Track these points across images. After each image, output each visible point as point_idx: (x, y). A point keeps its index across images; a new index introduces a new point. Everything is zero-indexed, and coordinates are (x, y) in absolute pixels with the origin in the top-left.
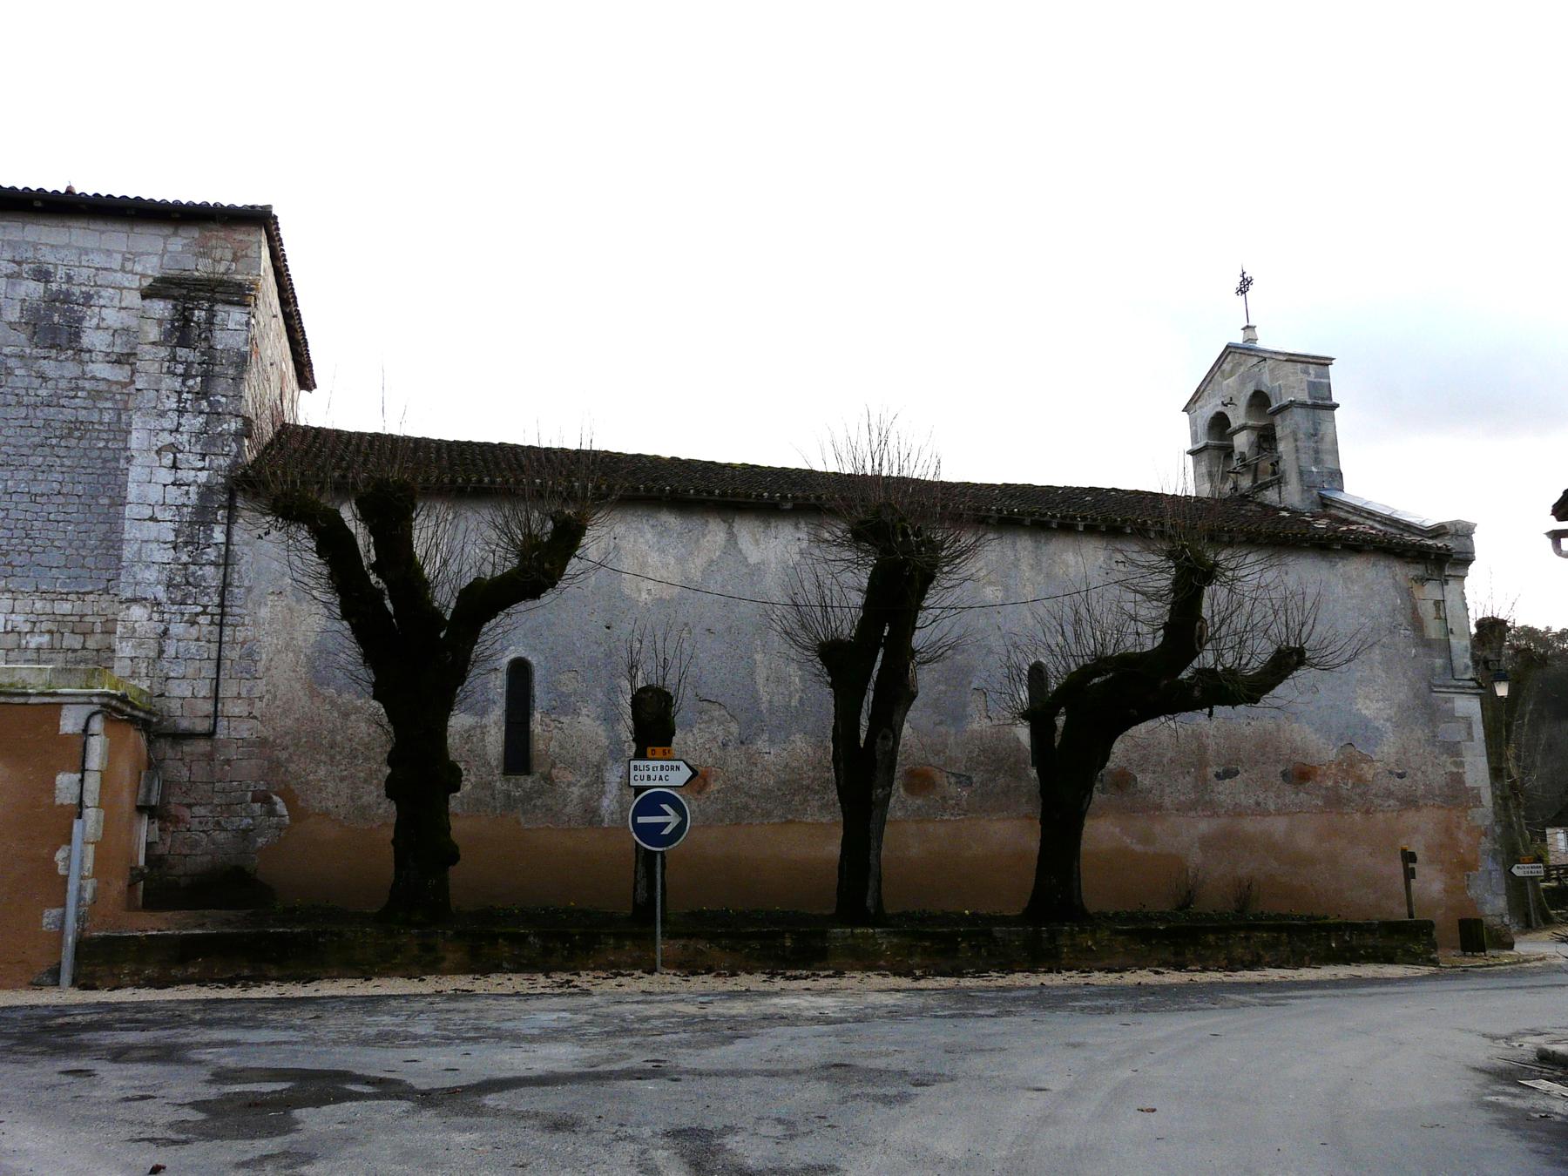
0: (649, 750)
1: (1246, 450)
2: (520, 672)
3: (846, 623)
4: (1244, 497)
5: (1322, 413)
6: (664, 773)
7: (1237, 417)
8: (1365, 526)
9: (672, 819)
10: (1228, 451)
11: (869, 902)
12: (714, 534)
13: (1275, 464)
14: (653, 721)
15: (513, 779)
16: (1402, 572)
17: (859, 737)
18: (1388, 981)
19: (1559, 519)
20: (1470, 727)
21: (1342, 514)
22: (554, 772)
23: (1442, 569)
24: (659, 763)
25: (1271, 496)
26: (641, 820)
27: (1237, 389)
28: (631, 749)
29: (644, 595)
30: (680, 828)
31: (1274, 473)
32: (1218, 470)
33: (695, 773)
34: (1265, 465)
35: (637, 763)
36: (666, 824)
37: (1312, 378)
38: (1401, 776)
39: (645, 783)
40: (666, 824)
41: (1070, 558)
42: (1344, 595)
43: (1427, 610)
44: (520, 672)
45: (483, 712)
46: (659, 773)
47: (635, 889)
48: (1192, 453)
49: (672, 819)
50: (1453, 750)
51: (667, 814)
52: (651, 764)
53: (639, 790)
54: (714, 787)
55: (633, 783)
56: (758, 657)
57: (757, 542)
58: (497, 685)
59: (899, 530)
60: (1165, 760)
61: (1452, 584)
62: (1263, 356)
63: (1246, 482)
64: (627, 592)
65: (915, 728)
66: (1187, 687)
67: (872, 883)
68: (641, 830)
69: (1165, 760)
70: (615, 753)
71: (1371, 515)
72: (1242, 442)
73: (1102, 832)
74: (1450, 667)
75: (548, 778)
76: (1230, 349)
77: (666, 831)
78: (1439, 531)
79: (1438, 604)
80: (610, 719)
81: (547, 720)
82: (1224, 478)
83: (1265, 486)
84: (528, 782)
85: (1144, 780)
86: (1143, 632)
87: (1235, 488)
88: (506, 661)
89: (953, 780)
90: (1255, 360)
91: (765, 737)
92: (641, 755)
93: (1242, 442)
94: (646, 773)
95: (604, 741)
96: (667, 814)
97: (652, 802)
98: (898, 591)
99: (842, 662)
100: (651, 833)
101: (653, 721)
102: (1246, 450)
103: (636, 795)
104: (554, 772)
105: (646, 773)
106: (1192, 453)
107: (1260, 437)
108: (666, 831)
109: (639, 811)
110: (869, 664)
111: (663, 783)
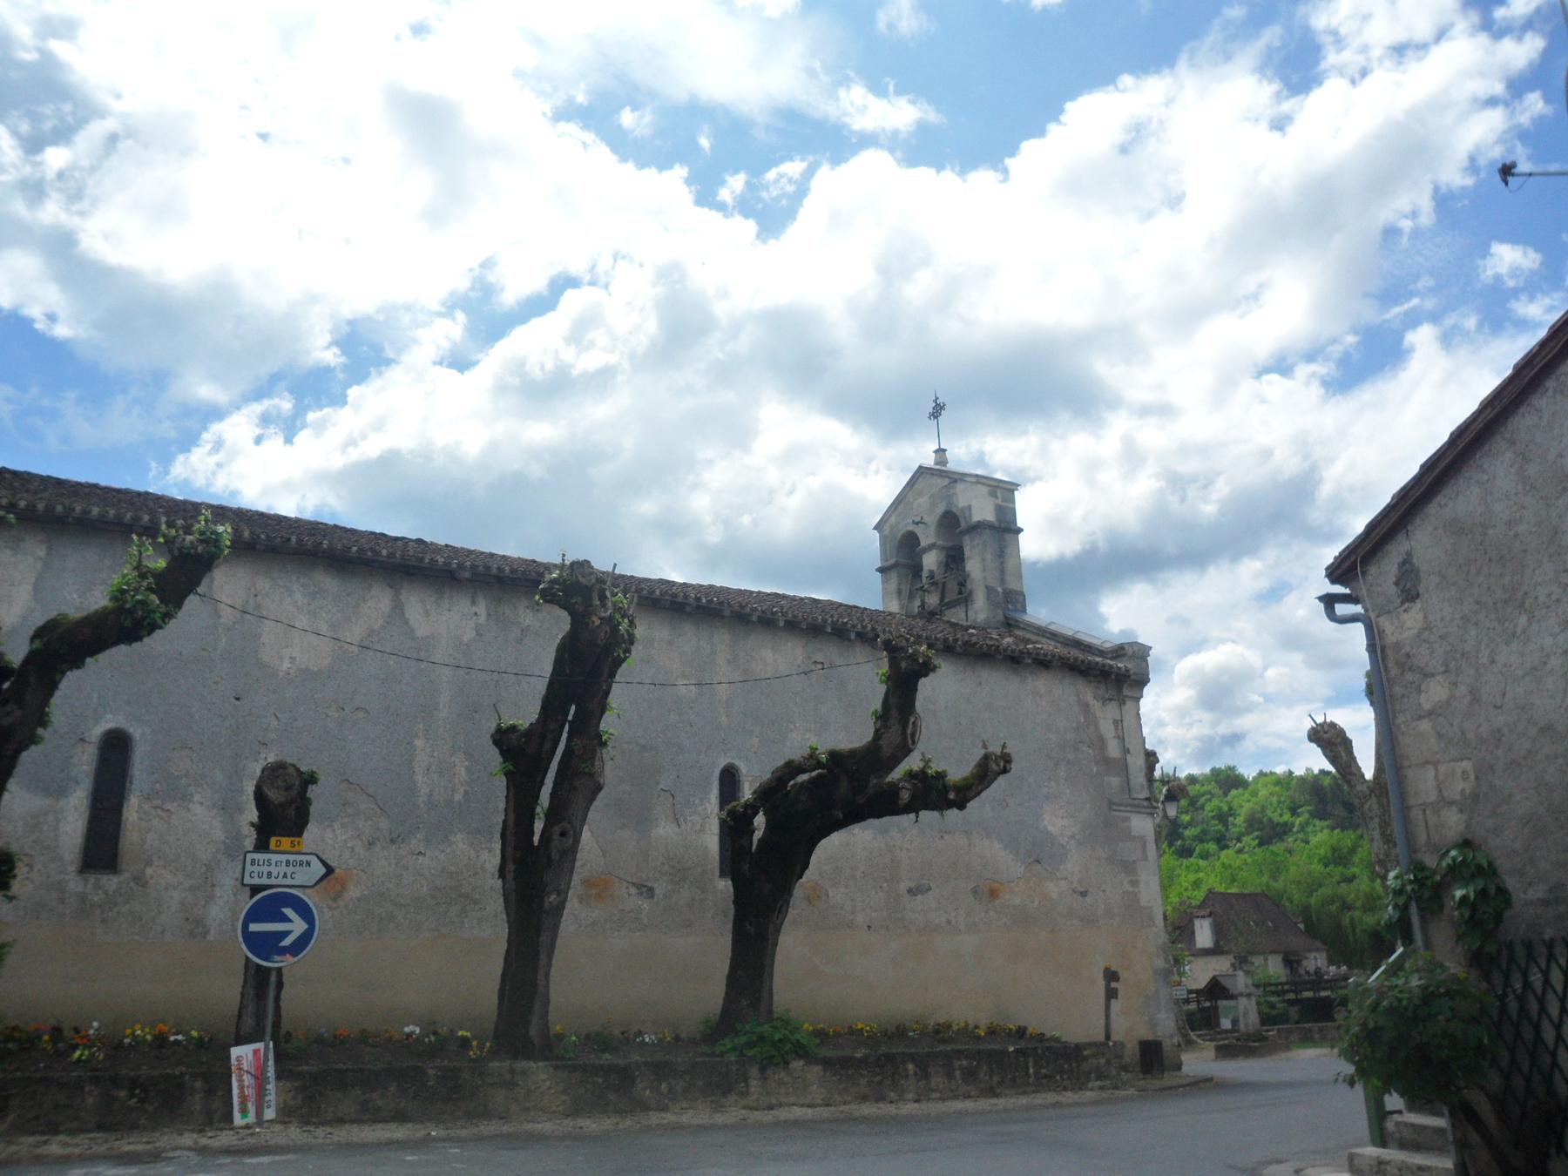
0: (273, 840)
1: (934, 568)
2: (116, 747)
3: (525, 714)
4: (932, 614)
5: (1008, 536)
6: (289, 870)
7: (927, 537)
8: (1047, 646)
9: (298, 926)
10: (916, 570)
11: (534, 1031)
12: (377, 601)
13: (962, 584)
14: (283, 809)
15: (92, 879)
16: (1088, 691)
17: (532, 833)
18: (364, 1147)
19: (1333, 582)
20: (1144, 846)
21: (1028, 636)
22: (149, 871)
23: (1120, 689)
24: (284, 858)
25: (956, 615)
26: (254, 927)
27: (928, 512)
28: (250, 837)
29: (286, 664)
30: (304, 939)
31: (960, 592)
32: (906, 588)
33: (330, 870)
34: (952, 586)
35: (257, 856)
36: (286, 934)
37: (999, 501)
38: (1084, 894)
39: (264, 881)
40: (286, 934)
41: (768, 654)
42: (1028, 711)
43: (1107, 729)
44: (116, 747)
45: (62, 792)
46: (283, 869)
47: (240, 1016)
48: (880, 570)
49: (298, 926)
50: (1129, 868)
51: (290, 921)
52: (274, 857)
53: (255, 890)
54: (353, 892)
55: (247, 880)
56: (419, 743)
57: (427, 612)
58: (85, 762)
59: (594, 621)
60: (858, 874)
61: (1129, 705)
62: (956, 478)
63: (933, 600)
64: (265, 658)
65: (595, 841)
66: (894, 790)
67: (537, 1007)
68: (252, 940)
69: (858, 874)
70: (231, 848)
71: (1053, 636)
72: (931, 561)
73: (794, 947)
74: (1127, 786)
75: (140, 880)
76: (922, 471)
77: (287, 942)
78: (1119, 651)
79: (1118, 723)
80: (228, 809)
81: (146, 807)
82: (911, 597)
83: (953, 604)
84: (110, 882)
85: (837, 895)
86: (849, 730)
87: (923, 606)
88: (98, 730)
89: (633, 890)
90: (946, 482)
91: (420, 836)
92: (262, 846)
93: (931, 561)
94: (265, 869)
95: (219, 834)
96: (290, 921)
97: (270, 904)
98: (585, 670)
99: (520, 754)
100: (265, 945)
101: (283, 809)
102: (934, 568)
103: (252, 897)
104: (149, 871)
105: (265, 869)
106: (880, 570)
107: (948, 556)
108: (287, 942)
109: (253, 916)
110: (549, 764)
111: (289, 881)
